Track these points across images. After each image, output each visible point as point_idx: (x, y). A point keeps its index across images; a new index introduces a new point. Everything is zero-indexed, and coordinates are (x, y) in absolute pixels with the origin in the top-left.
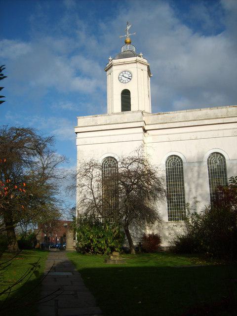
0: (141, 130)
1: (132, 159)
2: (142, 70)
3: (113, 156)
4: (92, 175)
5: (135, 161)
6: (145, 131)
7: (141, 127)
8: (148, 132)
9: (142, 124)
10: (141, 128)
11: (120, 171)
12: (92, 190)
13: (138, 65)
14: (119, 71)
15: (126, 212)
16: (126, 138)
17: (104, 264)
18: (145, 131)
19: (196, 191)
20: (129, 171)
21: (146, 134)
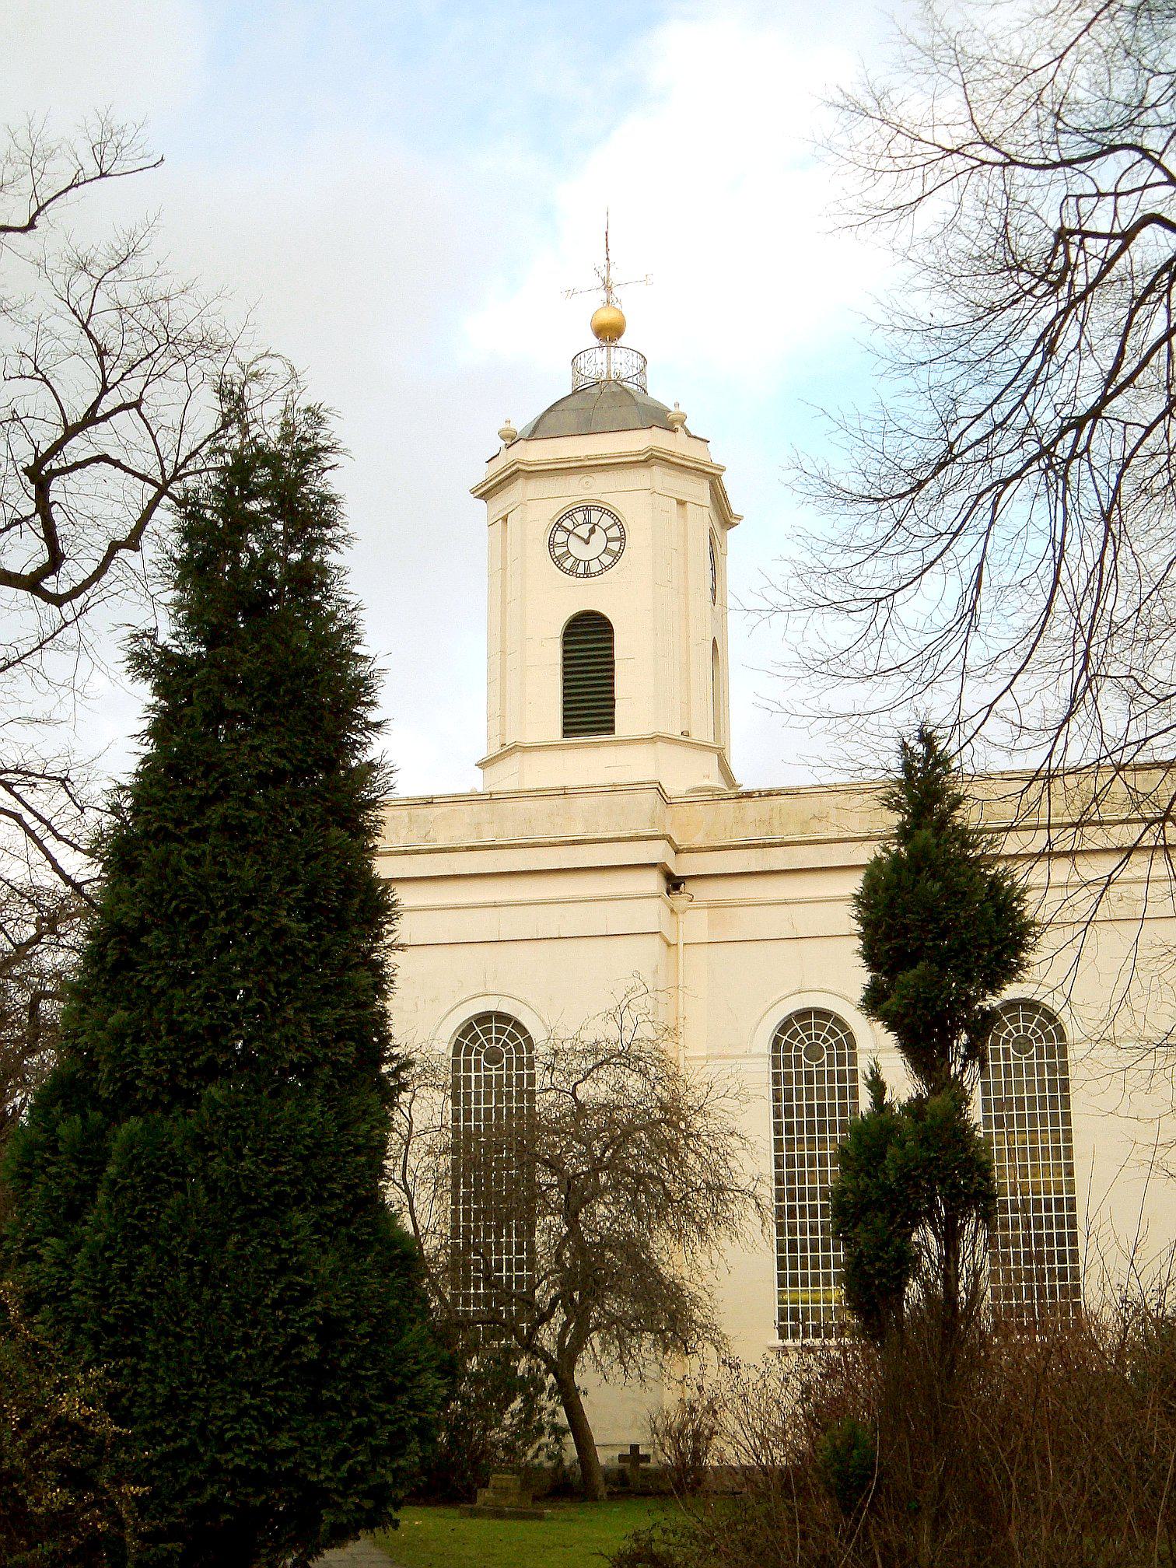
0: (653, 882)
1: (594, 1050)
2: (681, 503)
3: (505, 1008)
4: (411, 1123)
5: (606, 1062)
6: (674, 883)
7: (654, 865)
8: (690, 887)
9: (657, 852)
10: (657, 936)
11: (544, 1101)
12: (407, 1191)
13: (657, 476)
14: (553, 509)
15: (564, 1297)
16: (573, 920)
17: (601, 356)
18: (674, 883)
19: (934, 1540)
20: (581, 1106)
21: (680, 901)
